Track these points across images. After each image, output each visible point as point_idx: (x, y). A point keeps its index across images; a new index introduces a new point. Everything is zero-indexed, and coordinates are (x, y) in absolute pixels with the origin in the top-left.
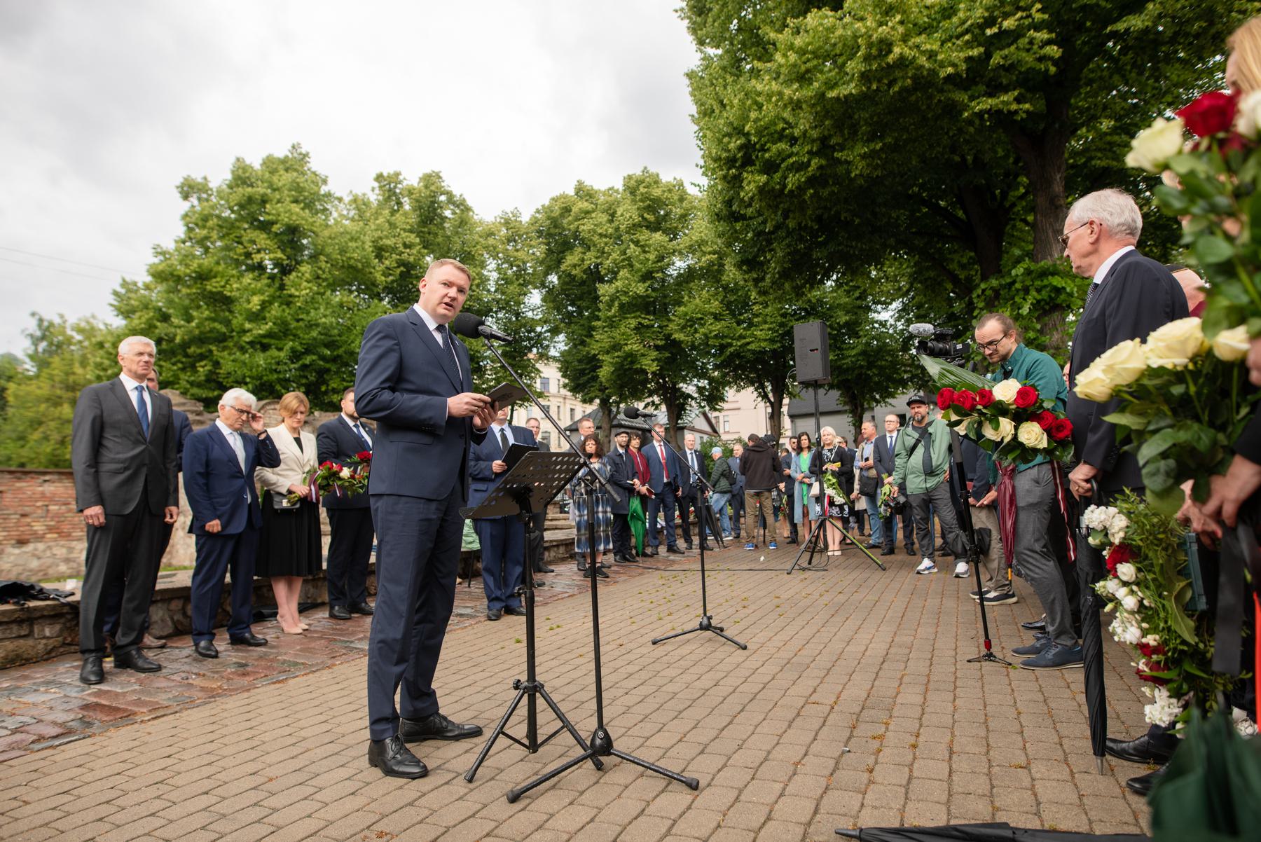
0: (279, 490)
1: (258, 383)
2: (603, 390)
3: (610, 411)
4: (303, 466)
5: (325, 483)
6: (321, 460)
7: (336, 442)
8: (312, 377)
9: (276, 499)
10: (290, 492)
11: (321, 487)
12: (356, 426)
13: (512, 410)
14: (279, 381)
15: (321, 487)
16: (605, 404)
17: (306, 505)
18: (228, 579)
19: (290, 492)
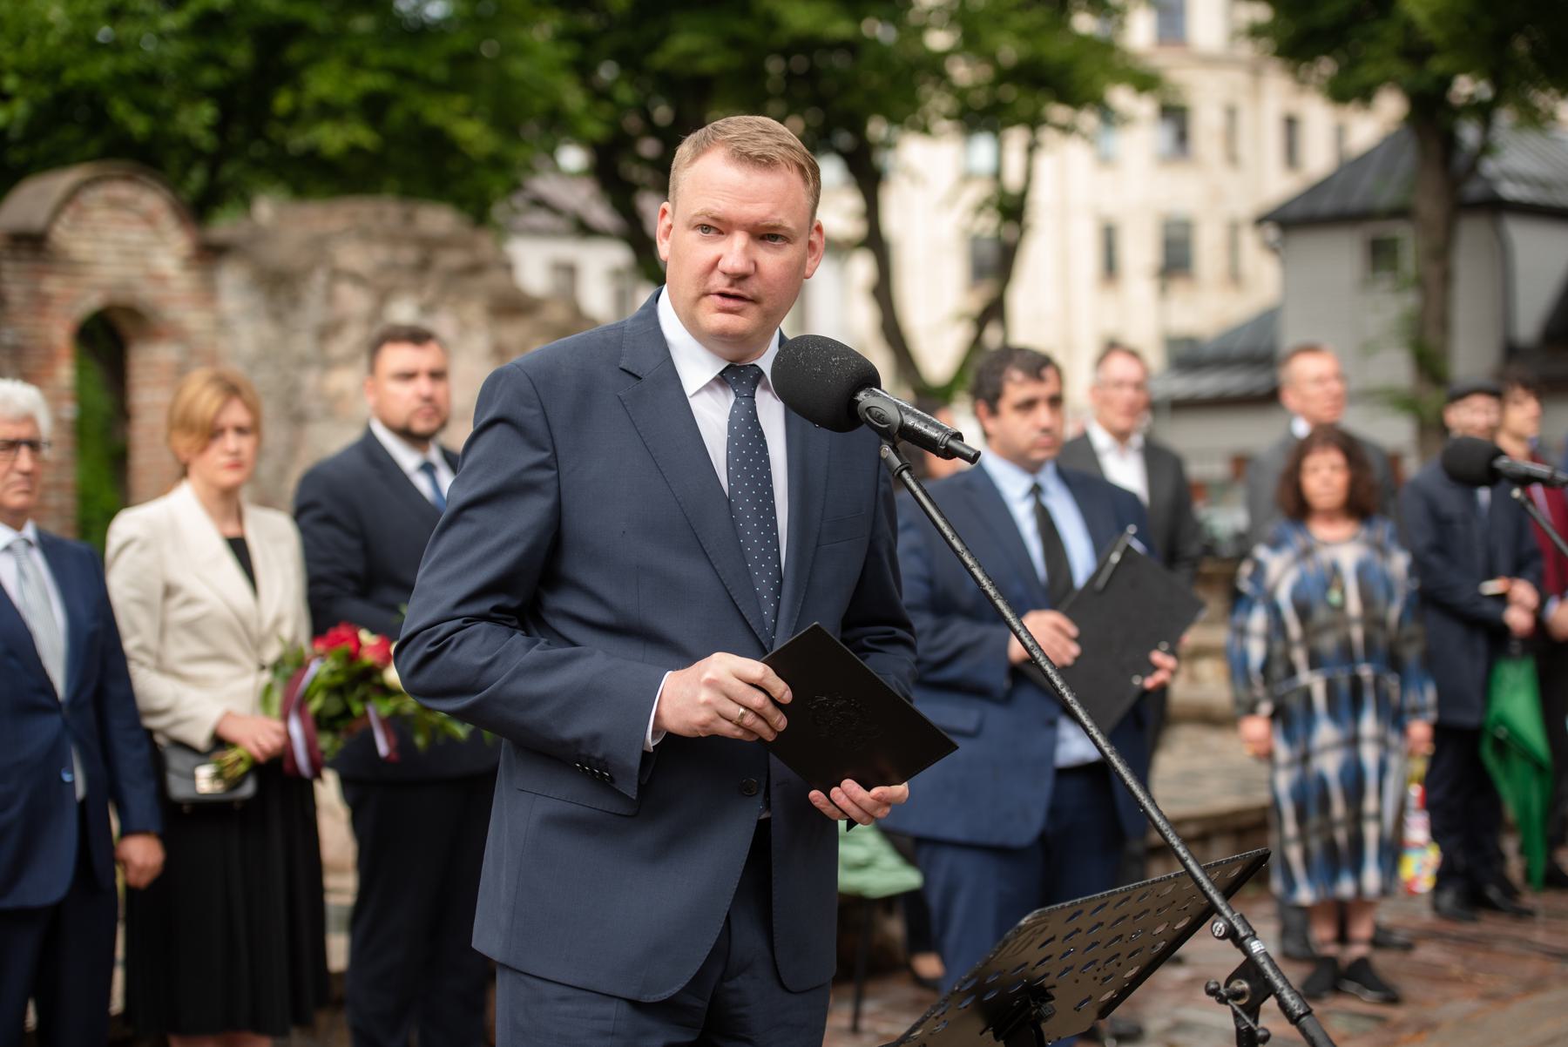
0: (181, 732)
1: (45, 92)
2: (1416, 52)
3: (1449, 142)
4: (257, 644)
5: (335, 706)
6: (323, 611)
7: (367, 549)
8: (241, 55)
9: (176, 760)
10: (220, 742)
11: (322, 723)
12: (428, 468)
13: (1032, 149)
14: (122, 81)
15: (322, 723)
16: (1430, 115)
17: (279, 784)
18: (31, 1018)
19: (220, 742)
